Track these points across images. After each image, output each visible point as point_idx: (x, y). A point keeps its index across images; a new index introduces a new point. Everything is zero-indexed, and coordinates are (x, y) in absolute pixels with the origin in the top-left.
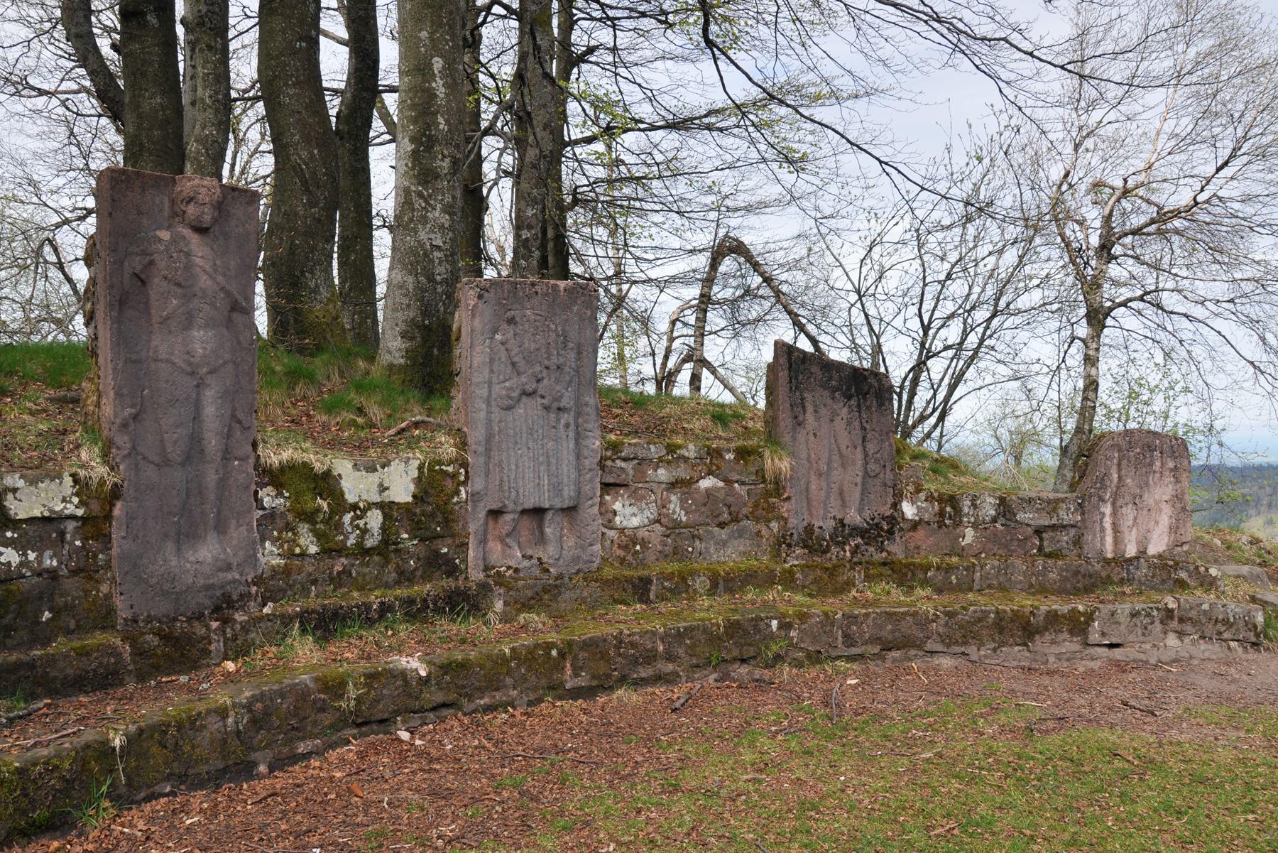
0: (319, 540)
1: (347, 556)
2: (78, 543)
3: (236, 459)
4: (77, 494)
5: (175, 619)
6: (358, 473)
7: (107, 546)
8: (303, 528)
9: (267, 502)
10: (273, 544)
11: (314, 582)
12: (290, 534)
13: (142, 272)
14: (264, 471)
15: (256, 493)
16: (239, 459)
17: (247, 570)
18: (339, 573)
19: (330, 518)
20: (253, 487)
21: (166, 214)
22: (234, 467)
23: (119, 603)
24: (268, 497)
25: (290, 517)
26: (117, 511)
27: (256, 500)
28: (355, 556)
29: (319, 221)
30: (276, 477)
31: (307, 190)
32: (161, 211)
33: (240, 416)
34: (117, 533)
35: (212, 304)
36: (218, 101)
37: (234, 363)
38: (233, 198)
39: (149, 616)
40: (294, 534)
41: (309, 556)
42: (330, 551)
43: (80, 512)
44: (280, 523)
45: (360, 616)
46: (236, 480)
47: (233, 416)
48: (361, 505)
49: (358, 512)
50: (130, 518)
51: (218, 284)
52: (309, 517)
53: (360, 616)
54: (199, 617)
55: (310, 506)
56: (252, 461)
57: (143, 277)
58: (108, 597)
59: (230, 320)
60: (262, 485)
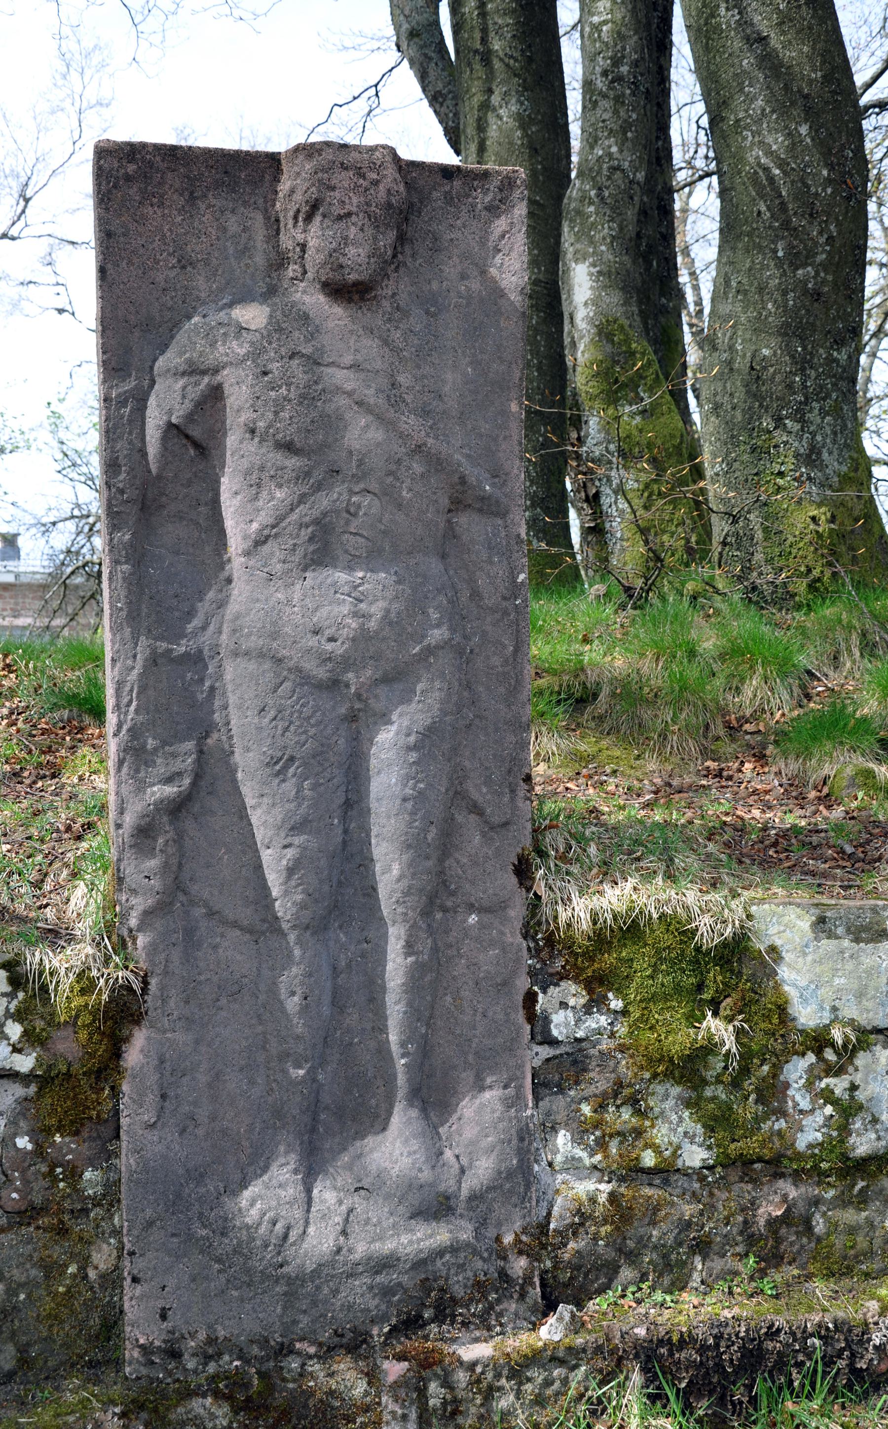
0: (710, 1129)
1: (797, 1177)
2: (23, 1142)
3: (471, 908)
4: (19, 1016)
5: (285, 1350)
6: (827, 945)
7: (106, 1154)
8: (666, 1099)
9: (561, 1024)
10: (578, 1139)
11: (702, 1247)
12: (626, 1114)
13: (190, 417)
14: (550, 940)
15: (530, 999)
16: (481, 910)
17: (499, 1211)
18: (773, 1223)
19: (745, 1071)
20: (523, 983)
21: (259, 259)
22: (466, 932)
23: (135, 1305)
24: (567, 1014)
25: (625, 1067)
26: (135, 1054)
27: (531, 1017)
28: (820, 1176)
29: (817, 295)
30: (594, 960)
31: (786, 225)
32: (245, 251)
33: (478, 792)
34: (135, 1113)
35: (388, 494)
36: (619, 79)
37: (460, 652)
38: (449, 199)
39: (211, 1341)
40: (638, 1112)
41: (684, 1172)
42: (750, 1164)
43: (25, 1063)
44: (599, 1082)
45: (828, 1362)
46: (473, 965)
47: (457, 795)
48: (837, 1035)
49: (830, 1055)
50: (169, 1070)
51: (403, 436)
52: (688, 1069)
53: (828, 1362)
54: (354, 1344)
55: (680, 1040)
56: (517, 912)
57: (195, 432)
58: (112, 1280)
59: (451, 533)
60: (546, 979)
